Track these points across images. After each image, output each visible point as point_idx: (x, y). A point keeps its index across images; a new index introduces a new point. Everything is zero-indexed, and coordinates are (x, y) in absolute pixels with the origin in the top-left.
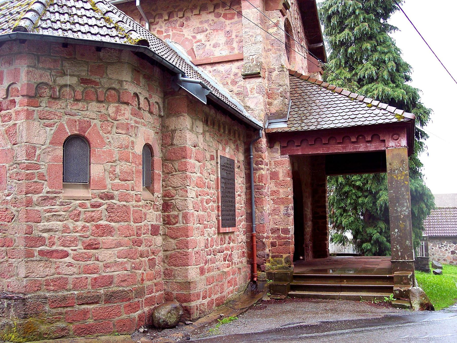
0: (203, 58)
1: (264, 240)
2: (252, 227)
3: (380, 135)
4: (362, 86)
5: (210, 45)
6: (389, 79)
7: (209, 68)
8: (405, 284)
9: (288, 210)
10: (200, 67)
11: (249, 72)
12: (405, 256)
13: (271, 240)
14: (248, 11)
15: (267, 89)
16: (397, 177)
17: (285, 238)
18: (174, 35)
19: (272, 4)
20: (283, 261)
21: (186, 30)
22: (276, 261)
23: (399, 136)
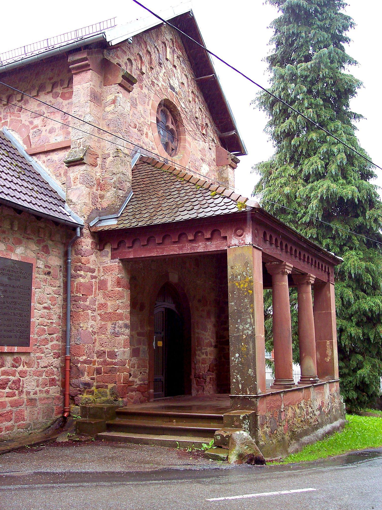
0: (38, 146)
1: (79, 365)
2: (66, 348)
3: (221, 231)
4: (308, 183)
5: (46, 130)
6: (340, 174)
7: (43, 157)
8: (236, 427)
9: (115, 328)
10: (34, 157)
11: (72, 159)
12: (246, 390)
13: (96, 366)
14: (79, 86)
15: (99, 179)
16: (240, 285)
17: (112, 363)
18: (12, 121)
19: (110, 78)
20: (108, 393)
21: (24, 114)
22: (100, 393)
23: (244, 231)
